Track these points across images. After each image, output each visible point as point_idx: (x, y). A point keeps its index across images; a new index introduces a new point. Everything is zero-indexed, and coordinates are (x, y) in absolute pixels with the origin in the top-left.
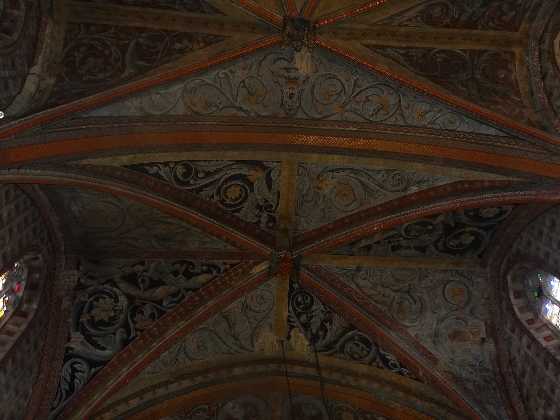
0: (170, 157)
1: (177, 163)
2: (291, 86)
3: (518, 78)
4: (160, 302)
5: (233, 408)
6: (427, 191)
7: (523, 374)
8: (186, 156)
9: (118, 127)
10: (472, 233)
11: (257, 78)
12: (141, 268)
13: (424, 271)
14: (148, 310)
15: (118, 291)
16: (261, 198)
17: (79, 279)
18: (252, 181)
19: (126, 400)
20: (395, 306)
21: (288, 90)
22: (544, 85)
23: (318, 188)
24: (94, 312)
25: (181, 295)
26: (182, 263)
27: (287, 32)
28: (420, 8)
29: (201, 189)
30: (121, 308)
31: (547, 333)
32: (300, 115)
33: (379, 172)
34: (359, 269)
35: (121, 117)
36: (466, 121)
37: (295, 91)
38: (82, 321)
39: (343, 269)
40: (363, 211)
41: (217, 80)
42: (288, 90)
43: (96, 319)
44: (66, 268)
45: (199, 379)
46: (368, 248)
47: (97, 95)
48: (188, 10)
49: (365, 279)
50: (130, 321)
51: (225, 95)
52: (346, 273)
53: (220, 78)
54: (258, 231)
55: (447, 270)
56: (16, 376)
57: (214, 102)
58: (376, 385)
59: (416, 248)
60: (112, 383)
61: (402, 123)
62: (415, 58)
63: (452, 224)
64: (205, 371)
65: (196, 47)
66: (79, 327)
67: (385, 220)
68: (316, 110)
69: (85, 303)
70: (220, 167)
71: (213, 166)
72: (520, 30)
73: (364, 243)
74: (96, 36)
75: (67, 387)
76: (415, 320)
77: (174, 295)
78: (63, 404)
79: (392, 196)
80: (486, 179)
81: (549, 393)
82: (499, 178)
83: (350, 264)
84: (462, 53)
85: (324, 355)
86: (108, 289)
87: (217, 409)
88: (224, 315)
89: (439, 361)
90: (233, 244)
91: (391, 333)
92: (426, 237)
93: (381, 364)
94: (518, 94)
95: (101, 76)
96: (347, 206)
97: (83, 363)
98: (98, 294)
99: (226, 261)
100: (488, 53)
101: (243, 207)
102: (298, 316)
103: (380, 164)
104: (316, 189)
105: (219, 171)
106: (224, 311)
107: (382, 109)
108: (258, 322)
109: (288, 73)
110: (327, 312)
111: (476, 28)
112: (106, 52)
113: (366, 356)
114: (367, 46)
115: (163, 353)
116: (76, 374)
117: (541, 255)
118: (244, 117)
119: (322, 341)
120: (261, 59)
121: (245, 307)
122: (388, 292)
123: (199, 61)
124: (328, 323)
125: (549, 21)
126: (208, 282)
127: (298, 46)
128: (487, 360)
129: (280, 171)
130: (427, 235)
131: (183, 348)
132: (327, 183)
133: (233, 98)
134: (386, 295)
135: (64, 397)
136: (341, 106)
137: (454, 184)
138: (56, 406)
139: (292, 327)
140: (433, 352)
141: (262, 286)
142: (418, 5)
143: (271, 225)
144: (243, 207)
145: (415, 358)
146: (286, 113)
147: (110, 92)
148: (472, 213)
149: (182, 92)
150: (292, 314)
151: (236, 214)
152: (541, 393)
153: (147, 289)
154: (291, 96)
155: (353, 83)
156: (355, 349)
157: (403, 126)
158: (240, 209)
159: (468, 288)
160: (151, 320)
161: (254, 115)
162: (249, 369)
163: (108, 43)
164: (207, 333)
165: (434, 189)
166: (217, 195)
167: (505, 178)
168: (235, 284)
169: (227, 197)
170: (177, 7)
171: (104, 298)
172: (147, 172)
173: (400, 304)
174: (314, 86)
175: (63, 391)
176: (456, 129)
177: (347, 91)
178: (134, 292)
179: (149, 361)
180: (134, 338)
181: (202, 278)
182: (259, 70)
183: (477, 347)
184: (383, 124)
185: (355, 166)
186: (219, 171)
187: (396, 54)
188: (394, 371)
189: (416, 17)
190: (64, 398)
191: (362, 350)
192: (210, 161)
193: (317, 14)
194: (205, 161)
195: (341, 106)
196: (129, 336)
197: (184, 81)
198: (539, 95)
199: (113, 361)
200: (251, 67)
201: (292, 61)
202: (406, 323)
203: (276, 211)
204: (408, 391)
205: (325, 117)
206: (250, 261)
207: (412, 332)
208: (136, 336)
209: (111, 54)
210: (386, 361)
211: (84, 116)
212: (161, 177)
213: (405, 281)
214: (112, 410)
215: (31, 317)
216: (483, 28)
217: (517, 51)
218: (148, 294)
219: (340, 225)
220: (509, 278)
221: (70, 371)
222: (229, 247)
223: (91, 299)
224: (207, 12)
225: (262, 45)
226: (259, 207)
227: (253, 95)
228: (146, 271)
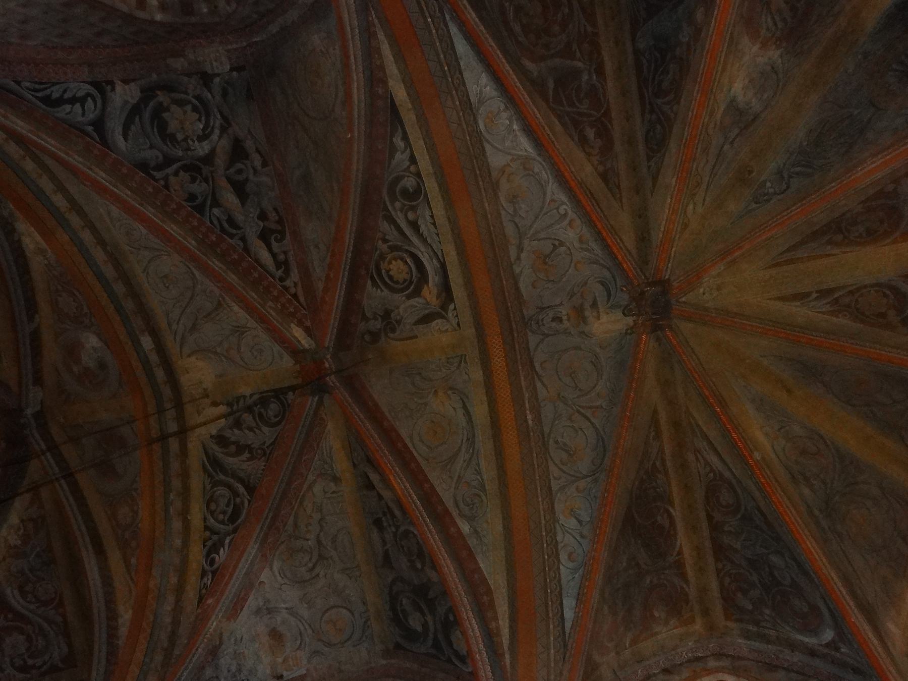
0: (424, 163)
1: (418, 175)
3: (659, 637)
4: (216, 203)
8: (431, 186)
9: (444, 71)
10: (425, 625)
11: (571, 262)
12: (258, 162)
13: (358, 573)
14: (198, 188)
15: (215, 137)
17: (218, 75)
18: (422, 294)
19: (61, 188)
21: (564, 312)
22: (655, 675)
25: (234, 231)
26: (280, 221)
27: (646, 289)
28: (727, 474)
30: (192, 148)
32: (533, 340)
33: (479, 473)
34: (336, 479)
35: (461, 73)
36: (577, 576)
37: (566, 324)
38: (158, 95)
40: (418, 465)
42: (564, 312)
43: (165, 115)
44: (228, 51)
46: (370, 486)
47: (482, 28)
49: (325, 493)
50: (175, 166)
52: (327, 463)
53: (557, 209)
55: (367, 605)
56: (47, 13)
58: (178, 542)
60: (76, 160)
61: (555, 486)
62: (654, 484)
63: (431, 595)
64: (135, 294)
66: (148, 93)
67: (412, 498)
68: (545, 361)
69: (186, 93)
70: (429, 241)
71: (429, 230)
72: (729, 624)
73: (374, 477)
75: (55, 95)
77: (231, 221)
79: (447, 497)
80: (501, 622)
82: (506, 641)
83: (342, 464)
85: (203, 461)
86: (214, 123)
88: (223, 303)
89: (235, 622)
91: (256, 546)
93: (209, 543)
94: (634, 642)
95: (517, 28)
97: (97, 112)
98: (203, 108)
103: (489, 472)
104: (433, 390)
105: (424, 241)
107: (570, 455)
109: (590, 306)
110: (263, 450)
113: (216, 520)
115: (143, 226)
116: (78, 105)
118: (509, 257)
119: (222, 453)
120: (602, 262)
121: (239, 331)
123: (573, 170)
124: (248, 455)
125: (749, 659)
127: (631, 310)
129: (447, 331)
130: (409, 564)
131: (158, 253)
134: (310, 528)
135: (39, 94)
136: (559, 395)
137: (484, 581)
138: (23, 86)
139: (229, 404)
141: (277, 348)
142: (730, 469)
144: (382, 291)
145: (229, 588)
147: (491, 46)
148: (451, 618)
149: (522, 156)
153: (229, 180)
156: (223, 502)
157: (550, 488)
158: (378, 287)
159: (348, 639)
161: (517, 272)
162: (154, 358)
165: (471, 555)
166: (389, 247)
167: (506, 648)
168: (270, 307)
169: (390, 263)
171: (200, 120)
175: (48, 92)
176: (563, 565)
178: (220, 161)
180: (153, 178)
181: (265, 256)
182: (584, 263)
183: (268, 671)
184: (547, 460)
186: (424, 241)
188: (204, 562)
189: (712, 470)
190: (37, 95)
191: (224, 513)
192: (434, 224)
193: (686, 327)
194: (432, 216)
196: (154, 169)
197: (539, 155)
198: (639, 671)
199: (268, 278)
200: (587, 250)
201: (610, 308)
202: (276, 565)
204: (180, 590)
206: (309, 321)
207: (265, 576)
208: (157, 181)
210: (215, 548)
211: (448, 17)
212: (392, 156)
213: (336, 549)
215: (140, 14)
216: (718, 571)
218: (223, 182)
219: (391, 436)
221: (80, 94)
222: (320, 285)
223: (194, 101)
224: (650, 164)
225: (620, 257)
228: (255, 171)
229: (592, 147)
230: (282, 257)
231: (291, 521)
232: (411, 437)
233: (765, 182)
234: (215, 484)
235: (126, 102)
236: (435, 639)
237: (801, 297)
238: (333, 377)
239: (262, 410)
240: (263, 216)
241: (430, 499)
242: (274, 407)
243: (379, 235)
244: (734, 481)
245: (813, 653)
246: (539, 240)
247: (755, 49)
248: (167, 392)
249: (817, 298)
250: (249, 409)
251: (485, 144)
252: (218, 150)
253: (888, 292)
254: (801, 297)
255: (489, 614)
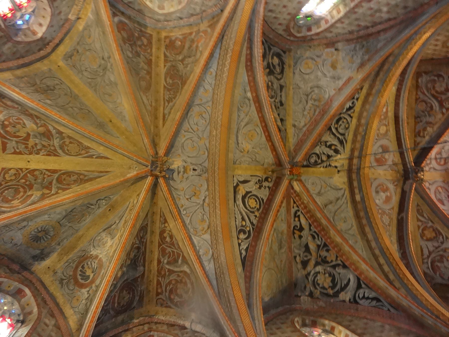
1: (238, 238)
2: (189, 171)
3: (180, 33)
4: (319, 246)
5: (379, 200)
6: (251, 87)
7: (359, 26)
8: (235, 234)
10: (272, 58)
12: (298, 259)
14: (324, 253)
16: (255, 187)
17: (306, 296)
20: (317, 103)
21: (191, 172)
22: (186, 18)
23: (248, 152)
24: (326, 286)
28: (142, 93)
29: (252, 223)
31: (335, 12)
33: (239, 116)
34: (294, 126)
37: (192, 167)
39: (294, 135)
40: (261, 123)
41: (188, 215)
42: (191, 172)
43: (331, 284)
44: (300, 304)
45: (364, 221)
46: (282, 120)
48: (146, 234)
50: (331, 264)
51: (196, 210)
54: (274, 188)
57: (201, 217)
59: (281, 91)
62: (170, 96)
63: (268, 70)
65: (168, 228)
66: (336, 295)
69: (320, 292)
70: (239, 212)
72: (151, 33)
73: (279, 123)
74: (164, 289)
76: (325, 92)
77: (314, 238)
78: (386, 304)
79: (253, 108)
81: (372, 11)
84: (166, 68)
85: (346, 146)
87: (380, 209)
90: (282, 202)
92: (275, 86)
93: (352, 111)
94: (191, 34)
96: (258, 134)
98: (315, 284)
99: (292, 207)
100: (166, 52)
101: (261, 197)
102: (322, 161)
106: (322, 207)
108: (327, 186)
111: (151, 60)
112: (173, 282)
114: (164, 125)
117: (288, 17)
120: (173, 189)
121: (319, 194)
122: (307, 107)
126: (305, 217)
128: (349, 47)
132: (245, 147)
133: (198, 205)
135: (381, 304)
136: (201, 140)
139: (330, 165)
140: (344, 80)
143: (270, 180)
144: (261, 197)
146: (205, 173)
150: (322, 165)
151: (265, 201)
152: (372, 15)
153: (311, 254)
154: (194, 170)
155: (187, 133)
156: (343, 126)
157: (213, 103)
160: (330, 252)
162: (357, 191)
163: (168, 281)
164: (336, 217)
165: (249, 83)
169: (255, 207)
170: (145, 241)
172: (245, 257)
173: (315, 100)
174: (189, 157)
177: (191, 136)
178: (312, 262)
179: (356, 252)
180: (342, 261)
185: (235, 130)
186: (241, 213)
187: (168, 108)
189: (147, 96)
194: (236, 221)
195: (201, 140)
202: (327, 96)
203: (262, 177)
205: (207, 150)
207: (333, 93)
209: (175, 279)
210: (350, 108)
212: (247, 248)
213: (301, 98)
214: (388, 274)
215: (334, 324)
216: (151, 55)
217: (164, 34)
218: (314, 254)
219: (269, 138)
220: (299, 35)
226: (260, 187)
227: (195, 193)
228: (300, 255)
229: (168, 234)
230: (297, 219)
231: (317, 113)
232: (261, 136)
233: (105, 205)
234: (343, 135)
235: (346, 293)
236: (270, 51)
237: (100, 157)
238: (287, 167)
239: (317, 160)
240: (300, 237)
241: (260, 109)
242: (312, 160)
243: (257, 219)
244: (9, 108)
245: (123, 13)
246: (196, 203)
247: (100, 256)
248: (354, 176)
249: (94, 155)
250: (322, 161)
251: (210, 243)
252: (313, 267)
253: (67, 151)
254: (100, 157)
255: (249, 57)
